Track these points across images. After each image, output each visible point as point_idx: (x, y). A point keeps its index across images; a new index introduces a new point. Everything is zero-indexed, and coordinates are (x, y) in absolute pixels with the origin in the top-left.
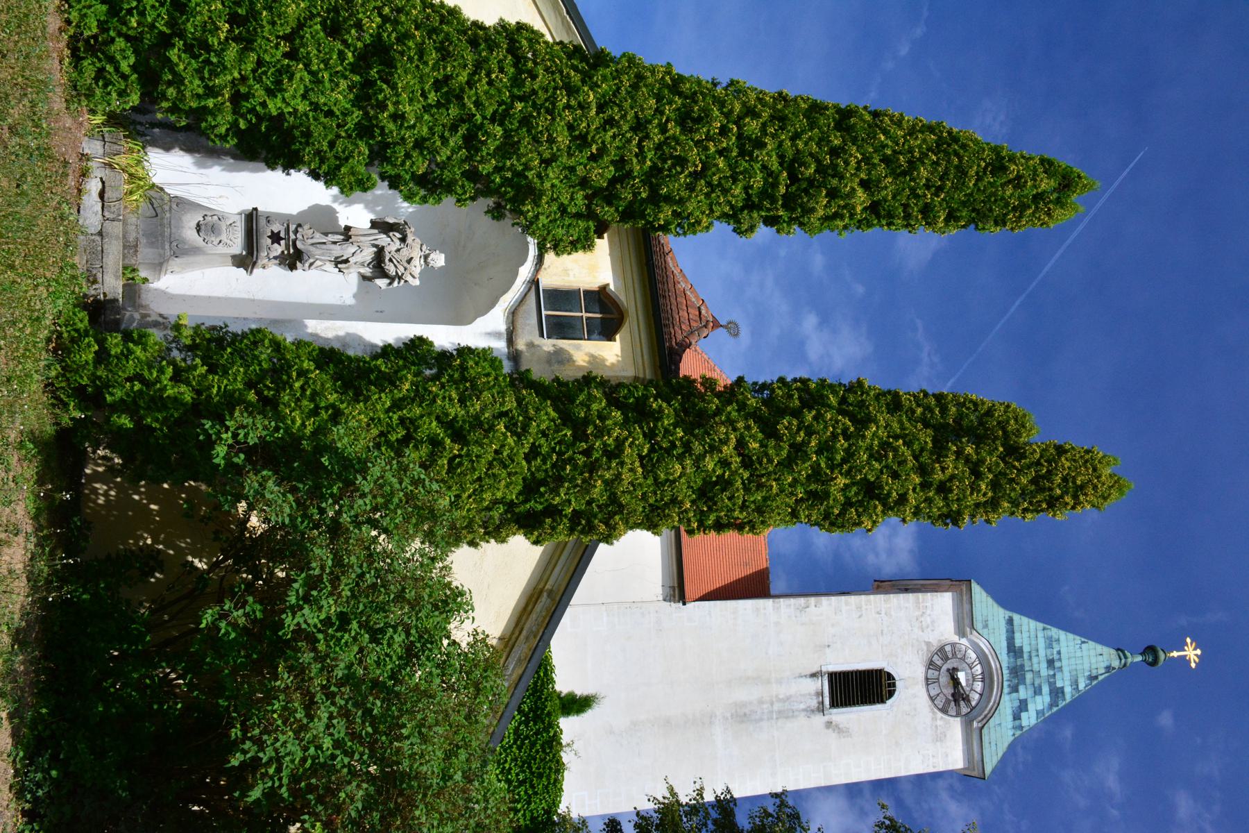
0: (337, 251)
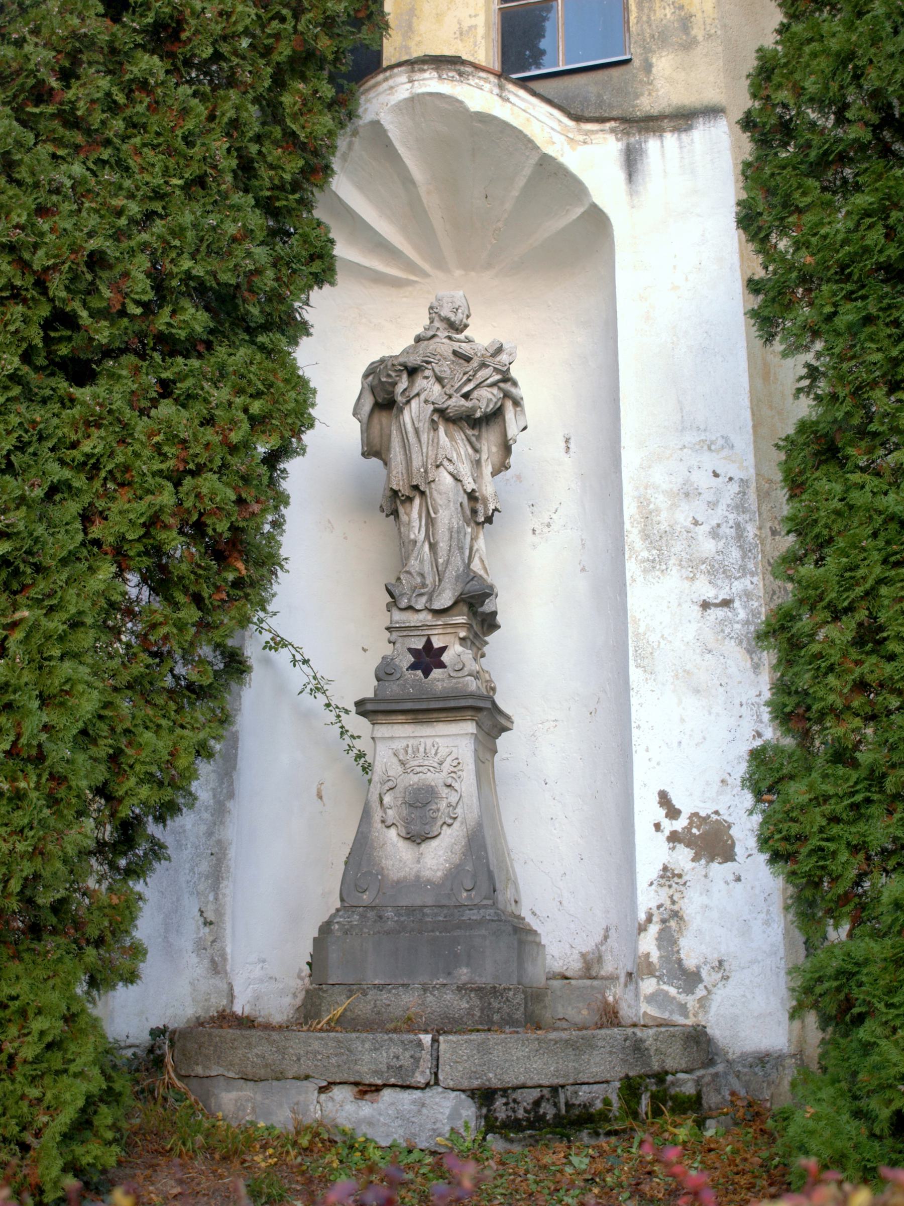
0: (448, 516)
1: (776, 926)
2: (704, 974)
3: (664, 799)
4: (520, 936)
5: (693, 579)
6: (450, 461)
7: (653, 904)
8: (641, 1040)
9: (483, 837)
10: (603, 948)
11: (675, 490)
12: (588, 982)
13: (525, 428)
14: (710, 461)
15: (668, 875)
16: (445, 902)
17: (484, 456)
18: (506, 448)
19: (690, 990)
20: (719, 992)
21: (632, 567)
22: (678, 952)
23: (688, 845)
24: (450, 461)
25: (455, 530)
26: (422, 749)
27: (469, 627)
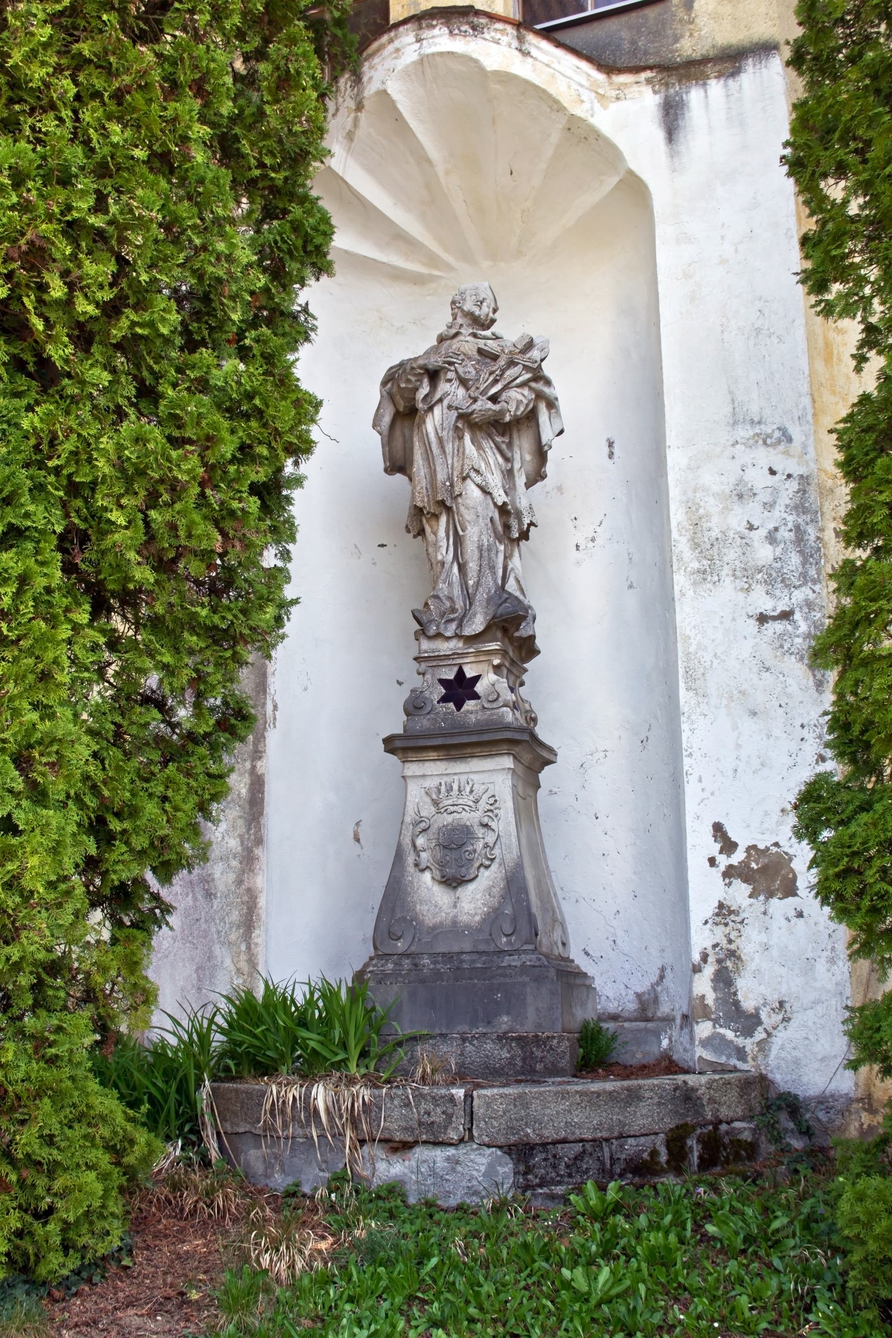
0: (476, 533)
1: (841, 964)
2: (763, 1015)
3: (718, 829)
4: (570, 979)
5: (748, 590)
6: (477, 471)
7: (708, 944)
8: (694, 1090)
9: (524, 878)
10: (659, 989)
11: (727, 491)
12: (642, 1025)
13: (561, 432)
14: (765, 457)
15: (724, 911)
16: (482, 947)
17: (517, 466)
18: (541, 454)
19: (748, 1032)
20: (779, 1034)
21: (680, 581)
22: (735, 994)
23: (746, 881)
24: (477, 471)
25: (485, 547)
26: (455, 787)
27: (503, 653)
